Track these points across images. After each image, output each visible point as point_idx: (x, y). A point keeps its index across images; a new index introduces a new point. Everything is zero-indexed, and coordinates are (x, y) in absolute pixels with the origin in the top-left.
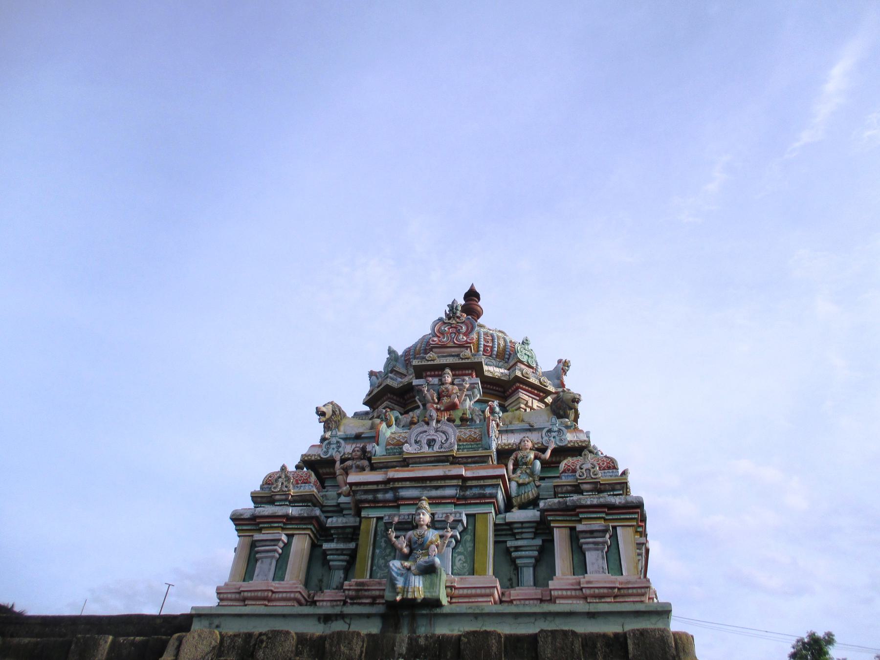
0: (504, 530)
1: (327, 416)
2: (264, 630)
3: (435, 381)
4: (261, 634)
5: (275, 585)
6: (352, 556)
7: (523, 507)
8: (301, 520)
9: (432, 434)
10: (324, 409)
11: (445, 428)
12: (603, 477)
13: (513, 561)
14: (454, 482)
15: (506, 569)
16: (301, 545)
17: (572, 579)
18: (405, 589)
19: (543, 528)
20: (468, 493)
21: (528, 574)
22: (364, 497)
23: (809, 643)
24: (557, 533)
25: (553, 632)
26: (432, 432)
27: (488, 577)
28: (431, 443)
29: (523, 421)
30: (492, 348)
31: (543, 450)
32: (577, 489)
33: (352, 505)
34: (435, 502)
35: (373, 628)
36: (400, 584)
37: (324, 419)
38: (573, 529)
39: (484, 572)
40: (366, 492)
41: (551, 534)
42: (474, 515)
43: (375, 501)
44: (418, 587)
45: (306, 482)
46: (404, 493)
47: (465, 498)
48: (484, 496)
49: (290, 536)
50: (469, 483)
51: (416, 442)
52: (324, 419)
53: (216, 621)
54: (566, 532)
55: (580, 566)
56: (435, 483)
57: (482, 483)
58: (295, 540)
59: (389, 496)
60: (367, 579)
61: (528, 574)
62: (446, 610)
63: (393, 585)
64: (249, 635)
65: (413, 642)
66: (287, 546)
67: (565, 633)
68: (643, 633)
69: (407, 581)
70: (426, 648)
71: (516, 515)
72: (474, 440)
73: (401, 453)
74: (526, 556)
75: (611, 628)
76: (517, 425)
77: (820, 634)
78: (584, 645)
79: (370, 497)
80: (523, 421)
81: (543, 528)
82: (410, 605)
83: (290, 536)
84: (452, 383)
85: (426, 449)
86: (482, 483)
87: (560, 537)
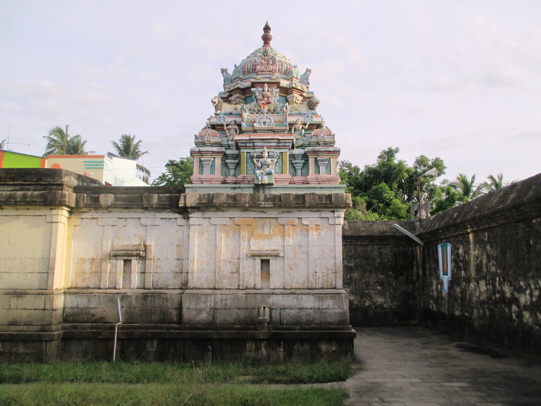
0: (292, 156)
1: (217, 103)
2: (214, 192)
3: (261, 89)
4: (213, 194)
5: (212, 176)
6: (238, 164)
7: (298, 147)
8: (218, 152)
9: (265, 119)
10: (214, 100)
11: (270, 117)
12: (328, 139)
13: (294, 167)
14: (275, 141)
15: (292, 170)
16: (218, 161)
17: (315, 176)
18: (262, 180)
19: (305, 156)
20: (280, 145)
21: (299, 172)
22: (241, 145)
23: (388, 152)
24: (310, 159)
25: (310, 194)
26: (265, 118)
27: (287, 175)
28: (264, 123)
29: (296, 110)
30: (282, 69)
31: (305, 125)
32: (318, 144)
33: (234, 145)
34: (269, 147)
35: (251, 191)
36: (260, 179)
37: (215, 105)
38: (316, 158)
39: (286, 173)
40: (242, 143)
41: (308, 160)
42: (282, 153)
43: (246, 146)
44: (266, 180)
45: (216, 136)
46: (256, 144)
47: (279, 146)
48: (286, 146)
49: (214, 158)
50: (280, 141)
51: (259, 122)
52: (215, 105)
53: (194, 189)
54: (314, 159)
55: (318, 171)
56: (268, 141)
57: (285, 141)
58: (216, 159)
59: (251, 145)
60: (245, 175)
61: (299, 172)
62: (274, 186)
63: (258, 179)
64: (209, 195)
65: (265, 196)
66: (213, 161)
67: (313, 194)
68: (337, 194)
69: (262, 177)
70: (270, 199)
71: (296, 151)
72: (281, 122)
73: (253, 126)
74: (299, 166)
75: (327, 192)
76: (294, 112)
77: (393, 148)
78: (319, 198)
79: (244, 145)
80: (296, 110)
81: (305, 156)
82: (263, 185)
83: (214, 158)
84: (268, 91)
85: (263, 126)
86: (285, 141)
87: (311, 161)
